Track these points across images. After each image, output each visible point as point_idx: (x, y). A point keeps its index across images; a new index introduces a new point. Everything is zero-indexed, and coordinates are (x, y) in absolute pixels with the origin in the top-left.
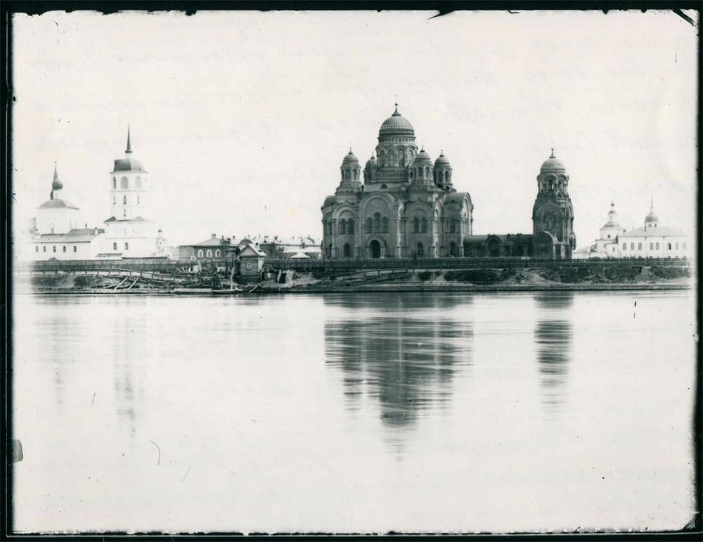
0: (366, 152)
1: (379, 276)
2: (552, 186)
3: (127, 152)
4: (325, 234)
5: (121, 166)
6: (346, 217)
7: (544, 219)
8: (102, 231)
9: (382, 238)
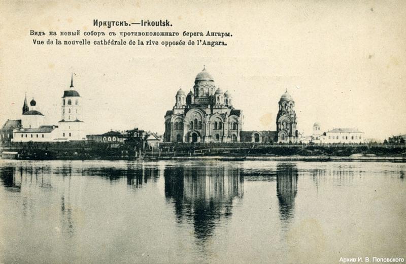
0: (188, 88)
1: (395, 159)
2: (284, 105)
3: (71, 87)
4: (166, 130)
5: (67, 94)
6: (218, 121)
7: (283, 123)
8: (57, 127)
9: (198, 132)
